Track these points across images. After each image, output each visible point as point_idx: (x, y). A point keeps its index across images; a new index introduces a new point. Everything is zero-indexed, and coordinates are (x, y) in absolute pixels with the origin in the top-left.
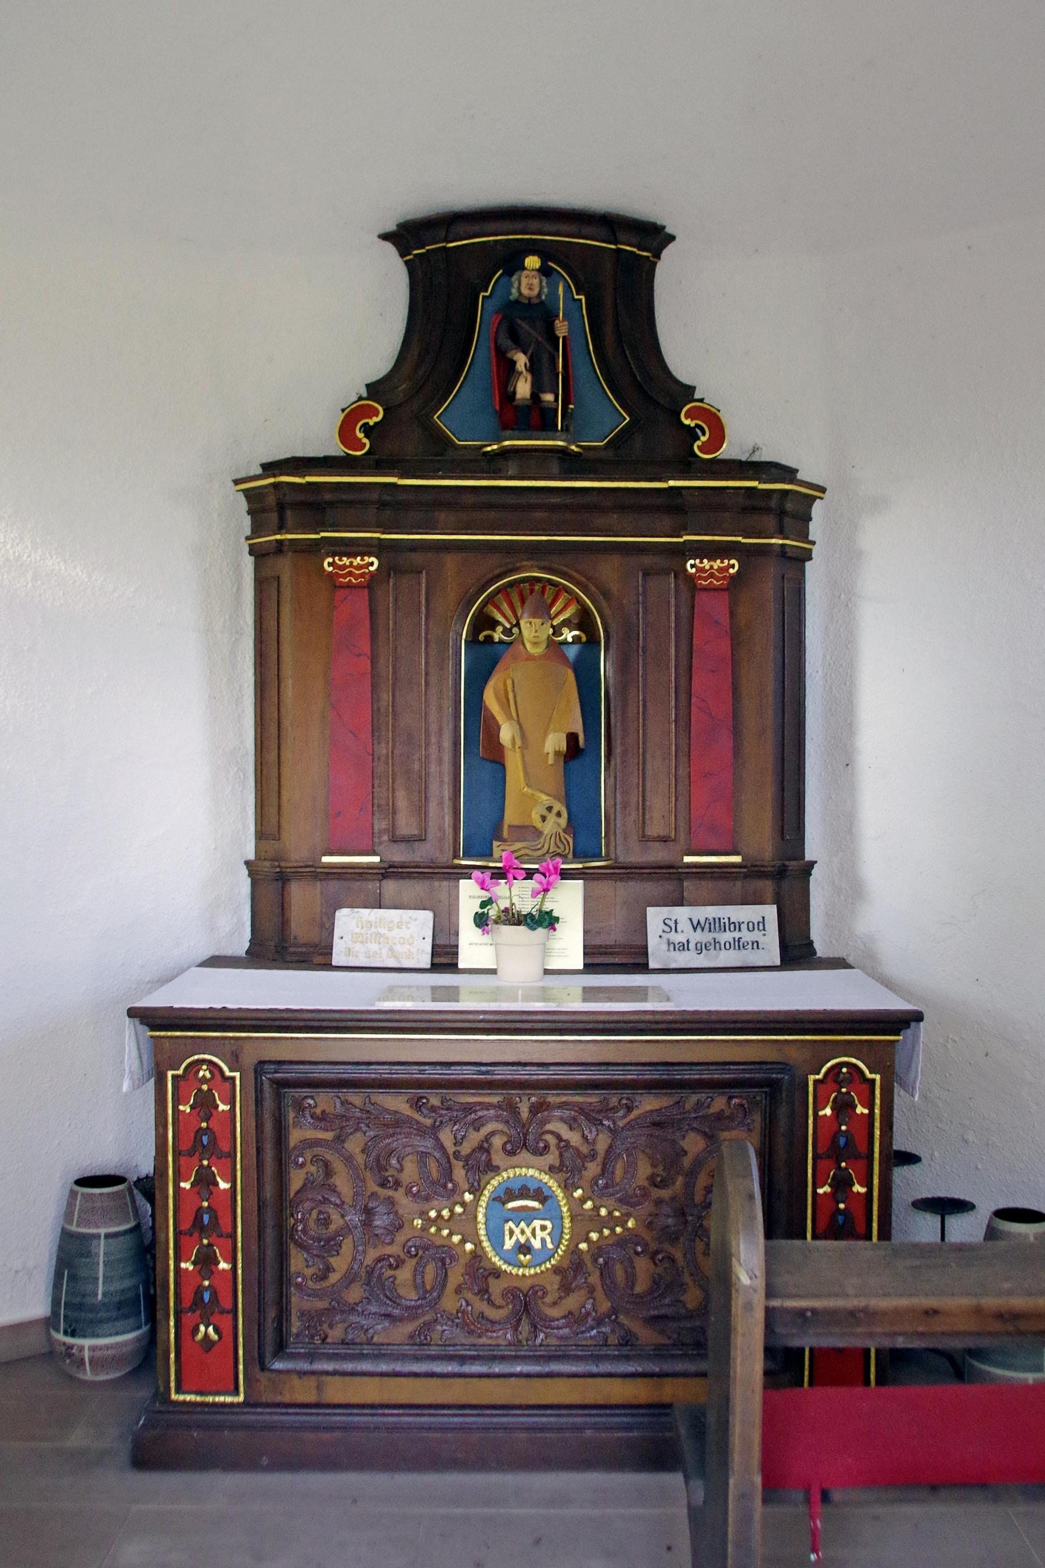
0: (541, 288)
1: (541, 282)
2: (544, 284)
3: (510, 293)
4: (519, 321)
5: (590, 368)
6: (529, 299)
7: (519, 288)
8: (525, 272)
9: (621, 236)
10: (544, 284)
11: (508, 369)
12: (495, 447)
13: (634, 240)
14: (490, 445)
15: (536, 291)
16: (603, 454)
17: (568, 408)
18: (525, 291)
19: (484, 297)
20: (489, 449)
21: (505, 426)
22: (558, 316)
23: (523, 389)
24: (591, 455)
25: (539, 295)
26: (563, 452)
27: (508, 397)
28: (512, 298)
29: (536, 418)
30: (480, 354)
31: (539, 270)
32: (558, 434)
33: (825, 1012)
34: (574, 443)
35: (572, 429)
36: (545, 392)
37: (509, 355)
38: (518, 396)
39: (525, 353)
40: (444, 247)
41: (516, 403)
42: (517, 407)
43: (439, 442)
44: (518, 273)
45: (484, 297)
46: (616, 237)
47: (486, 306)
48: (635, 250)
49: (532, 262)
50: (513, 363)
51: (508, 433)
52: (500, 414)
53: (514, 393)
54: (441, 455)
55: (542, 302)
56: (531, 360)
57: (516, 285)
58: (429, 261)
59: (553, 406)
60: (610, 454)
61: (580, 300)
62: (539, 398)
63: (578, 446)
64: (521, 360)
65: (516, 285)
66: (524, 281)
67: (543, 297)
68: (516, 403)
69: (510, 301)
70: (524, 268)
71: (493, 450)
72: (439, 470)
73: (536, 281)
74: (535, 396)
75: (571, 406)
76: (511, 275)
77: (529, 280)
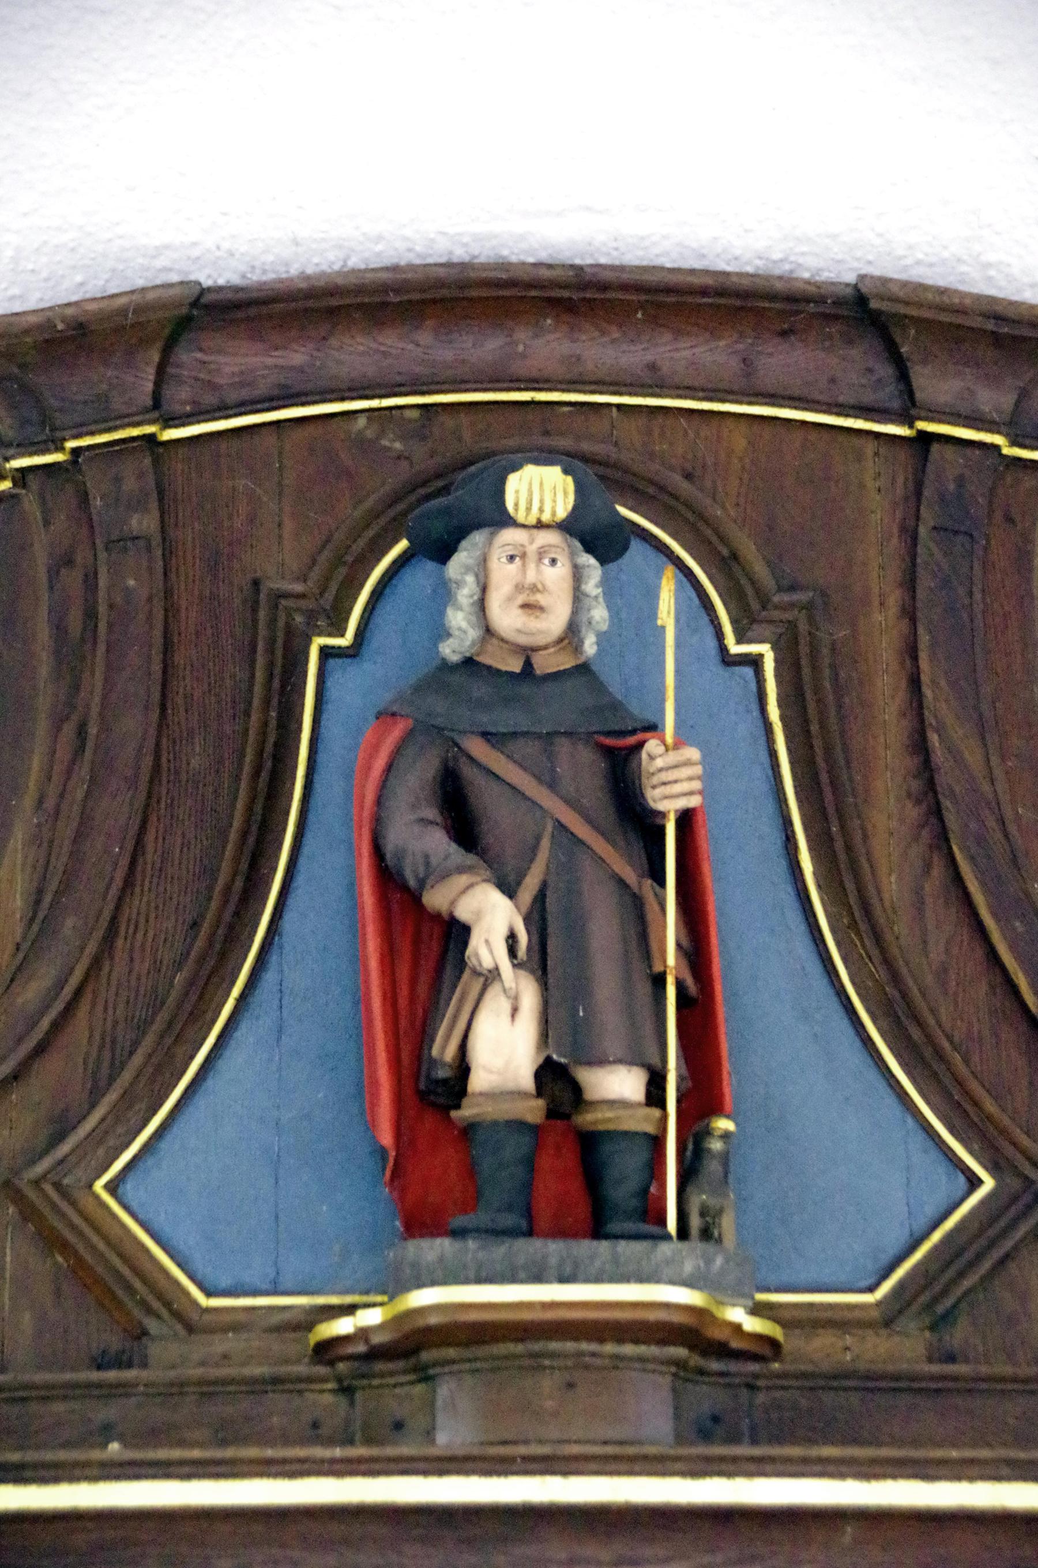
0: (578, 596)
1: (577, 575)
2: (592, 586)
3: (443, 633)
4: (477, 747)
5: (803, 947)
6: (527, 653)
7: (481, 605)
8: (509, 536)
9: (933, 383)
10: (592, 586)
11: (429, 954)
12: (371, 1317)
13: (994, 399)
14: (350, 1309)
15: (554, 622)
16: (876, 1350)
17: (14, 1202)
18: (507, 619)
19: (326, 653)
20: (343, 1326)
21: (419, 1222)
22: (653, 728)
23: (502, 1045)
24: (823, 1349)
25: (572, 633)
26: (693, 1338)
27: (435, 1090)
28: (450, 650)
29: (575, 1179)
30: (315, 919)
31: (566, 527)
32: (665, 1249)
33: (689, 1505)
34: (737, 1293)
35: (727, 1224)
36: (602, 1062)
37: (436, 899)
38: (479, 1081)
39: (509, 891)
40: (151, 438)
41: (466, 1112)
42: (469, 1131)
43: (114, 1298)
44: (478, 538)
45: (326, 653)
46: (909, 392)
47: (343, 712)
48: (998, 439)
49: (539, 490)
50: (456, 933)
51: (434, 1249)
52: (399, 1170)
53: (463, 1068)
54: (121, 1362)
55: (584, 669)
56: (537, 918)
57: (466, 593)
58: (84, 499)
59: (643, 1121)
60: (907, 1349)
61: (755, 662)
62: (577, 1089)
63: (758, 1310)
64: (492, 918)
65: (466, 593)
66: (504, 575)
67: (590, 647)
68: (466, 1112)
69: (445, 667)
70: (504, 520)
71: (363, 1333)
72: (107, 1432)
73: (556, 577)
74: (555, 1079)
75: (723, 1124)
76: (443, 552)
77: (523, 579)
